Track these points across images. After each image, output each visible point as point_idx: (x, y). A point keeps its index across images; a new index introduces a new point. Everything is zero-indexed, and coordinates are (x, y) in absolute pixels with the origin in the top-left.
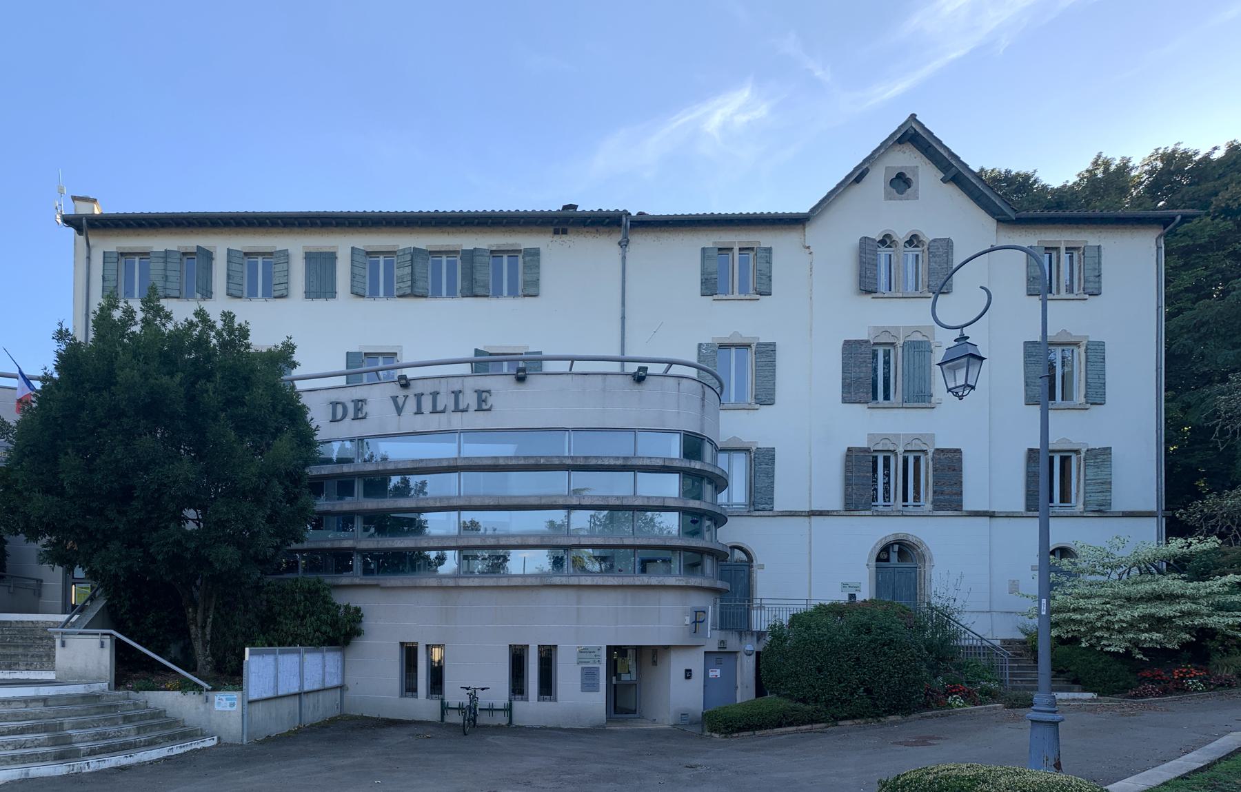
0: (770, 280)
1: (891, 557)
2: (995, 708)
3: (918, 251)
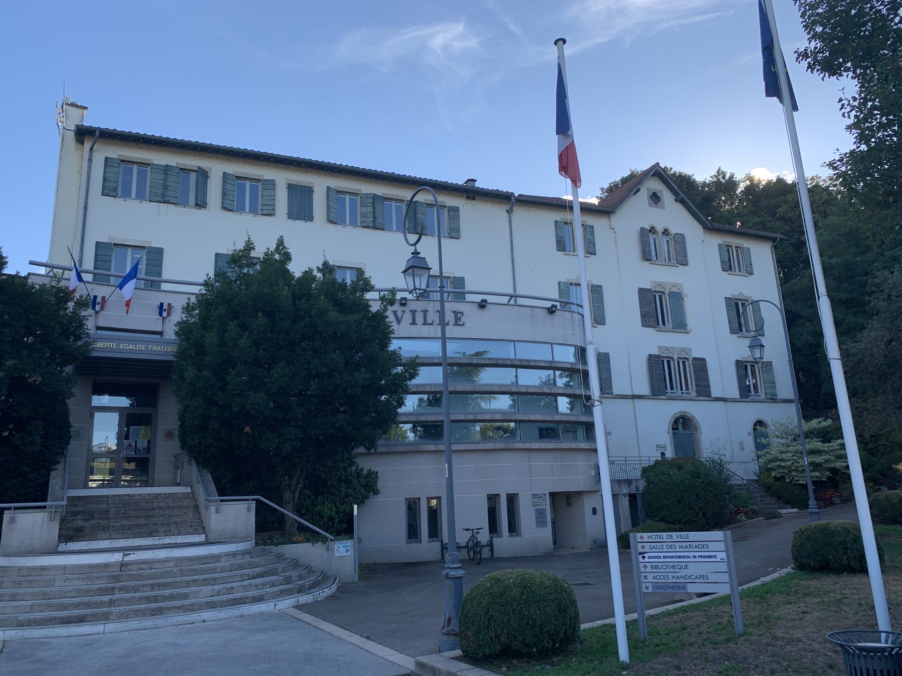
0: (595, 246)
1: (679, 427)
2: (760, 520)
3: (668, 238)
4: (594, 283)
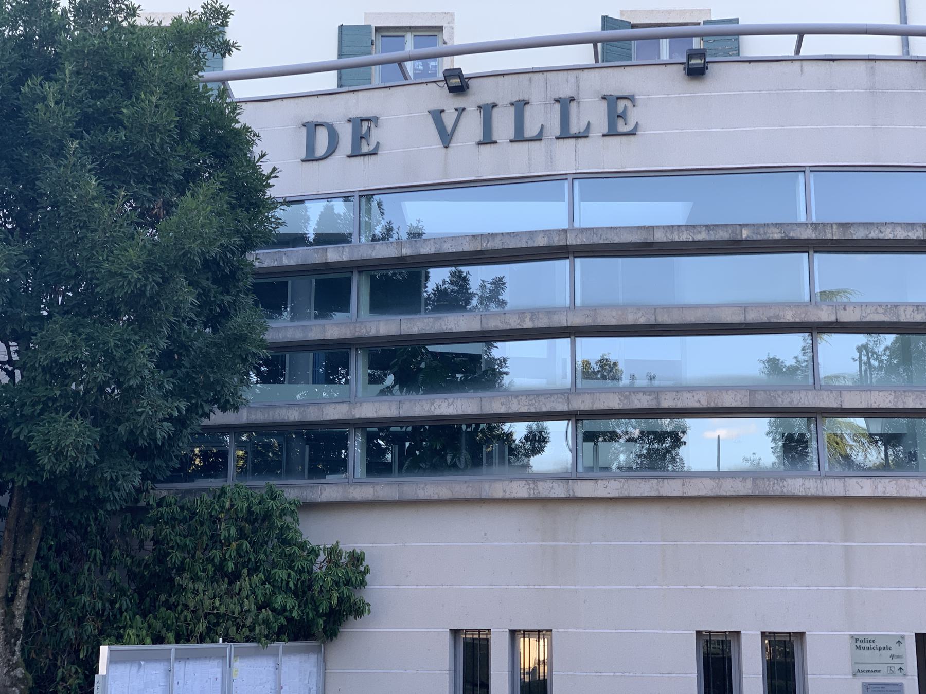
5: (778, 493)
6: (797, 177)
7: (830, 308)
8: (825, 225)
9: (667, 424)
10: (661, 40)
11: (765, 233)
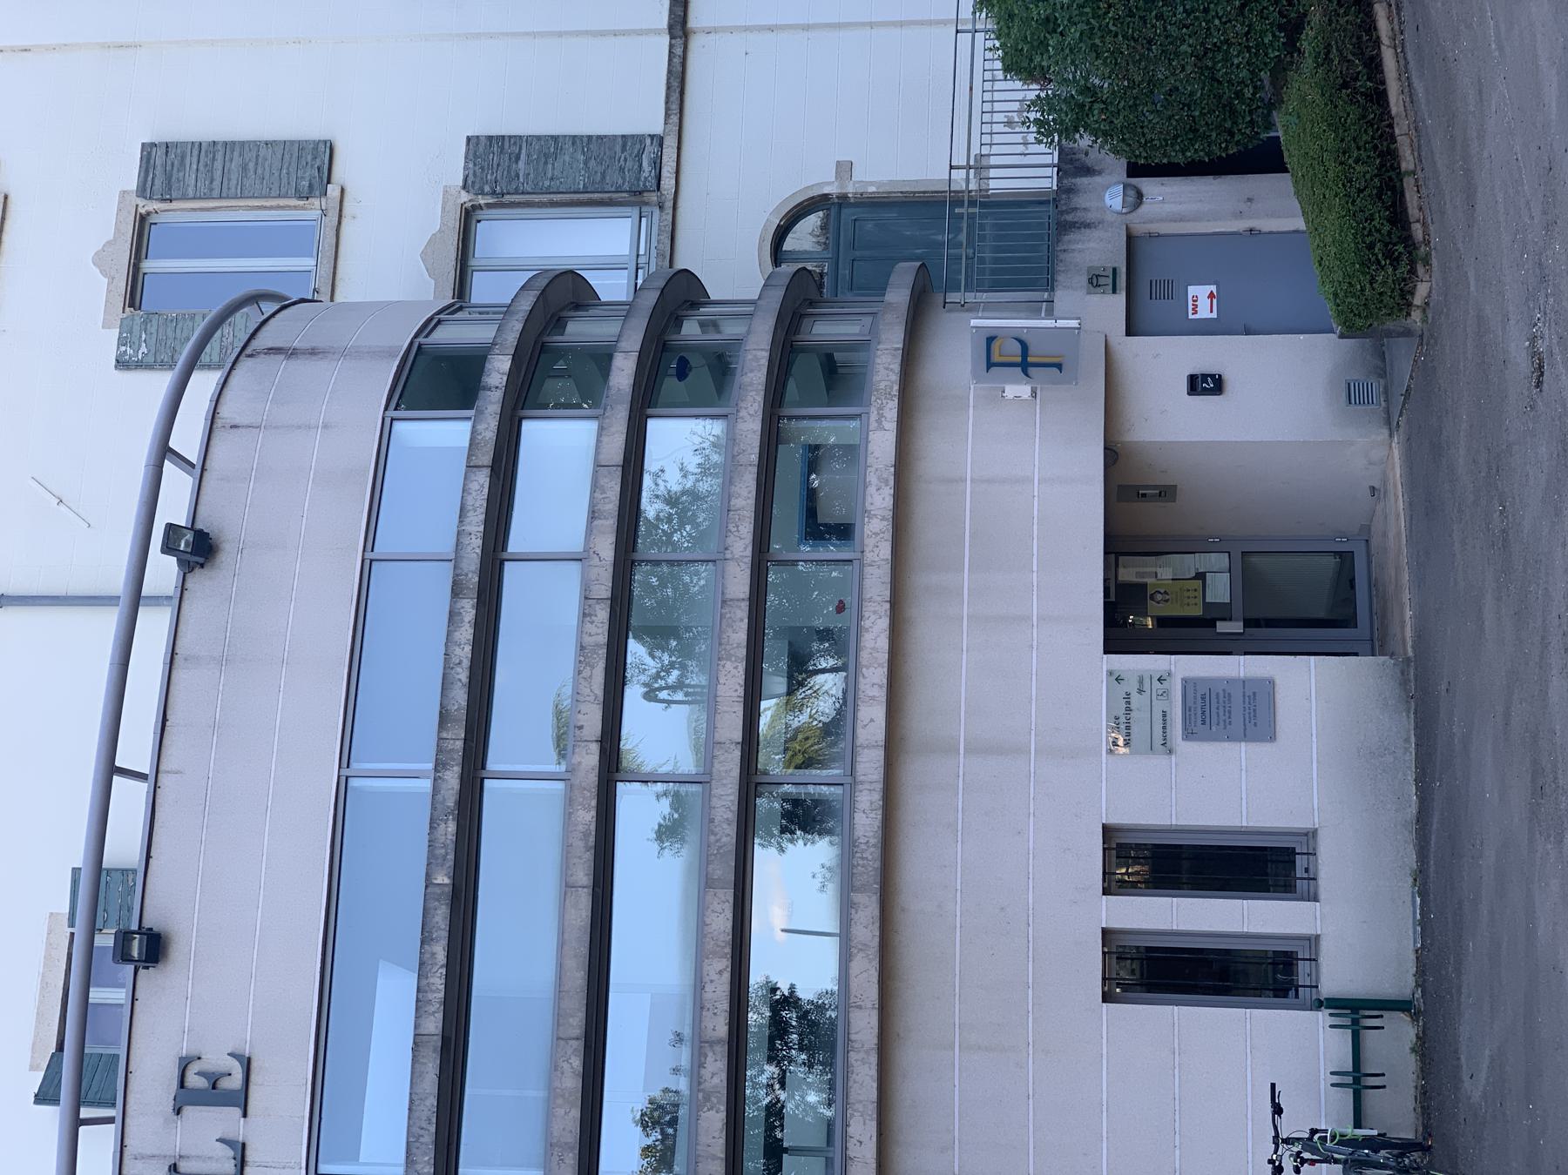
4: (133, 185)
5: (877, 853)
6: (355, 789)
7: (577, 750)
8: (440, 750)
9: (757, 1017)
10: (91, 1001)
11: (445, 846)
